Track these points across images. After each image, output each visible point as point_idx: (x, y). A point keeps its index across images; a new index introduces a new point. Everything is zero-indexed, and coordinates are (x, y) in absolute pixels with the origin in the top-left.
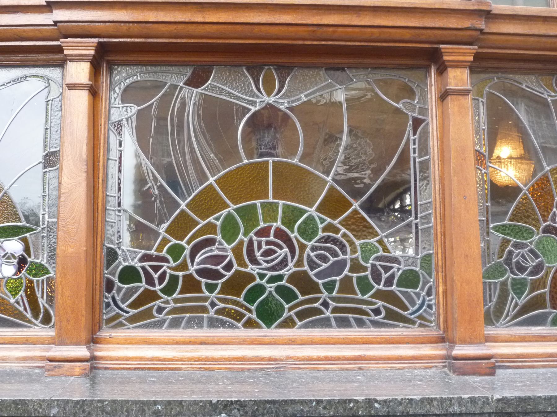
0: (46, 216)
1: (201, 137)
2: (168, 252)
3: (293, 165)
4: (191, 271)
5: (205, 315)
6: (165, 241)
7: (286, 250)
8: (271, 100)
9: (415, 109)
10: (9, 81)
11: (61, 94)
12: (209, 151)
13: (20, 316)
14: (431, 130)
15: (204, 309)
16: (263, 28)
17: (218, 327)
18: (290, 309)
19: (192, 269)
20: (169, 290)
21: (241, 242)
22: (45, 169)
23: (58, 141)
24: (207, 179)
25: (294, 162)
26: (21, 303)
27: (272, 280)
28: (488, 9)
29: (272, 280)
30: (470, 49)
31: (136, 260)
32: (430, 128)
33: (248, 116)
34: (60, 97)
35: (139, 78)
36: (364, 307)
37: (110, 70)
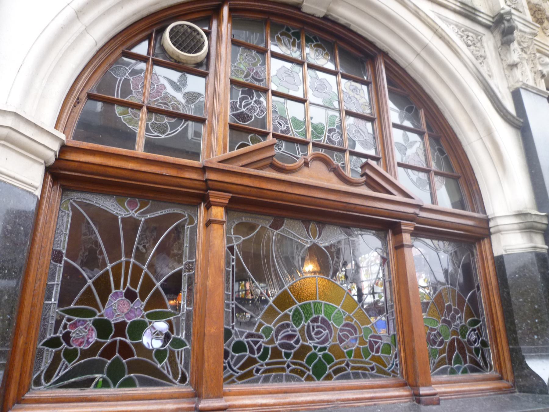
0: (185, 306)
2: (263, 331)
4: (276, 345)
5: (284, 373)
6: (261, 325)
7: (327, 331)
13: (164, 377)
15: (283, 370)
17: (290, 381)
18: (330, 368)
19: (277, 343)
20: (263, 358)
21: (303, 327)
26: (166, 368)
27: (321, 350)
29: (321, 350)
31: (243, 337)
36: (366, 366)
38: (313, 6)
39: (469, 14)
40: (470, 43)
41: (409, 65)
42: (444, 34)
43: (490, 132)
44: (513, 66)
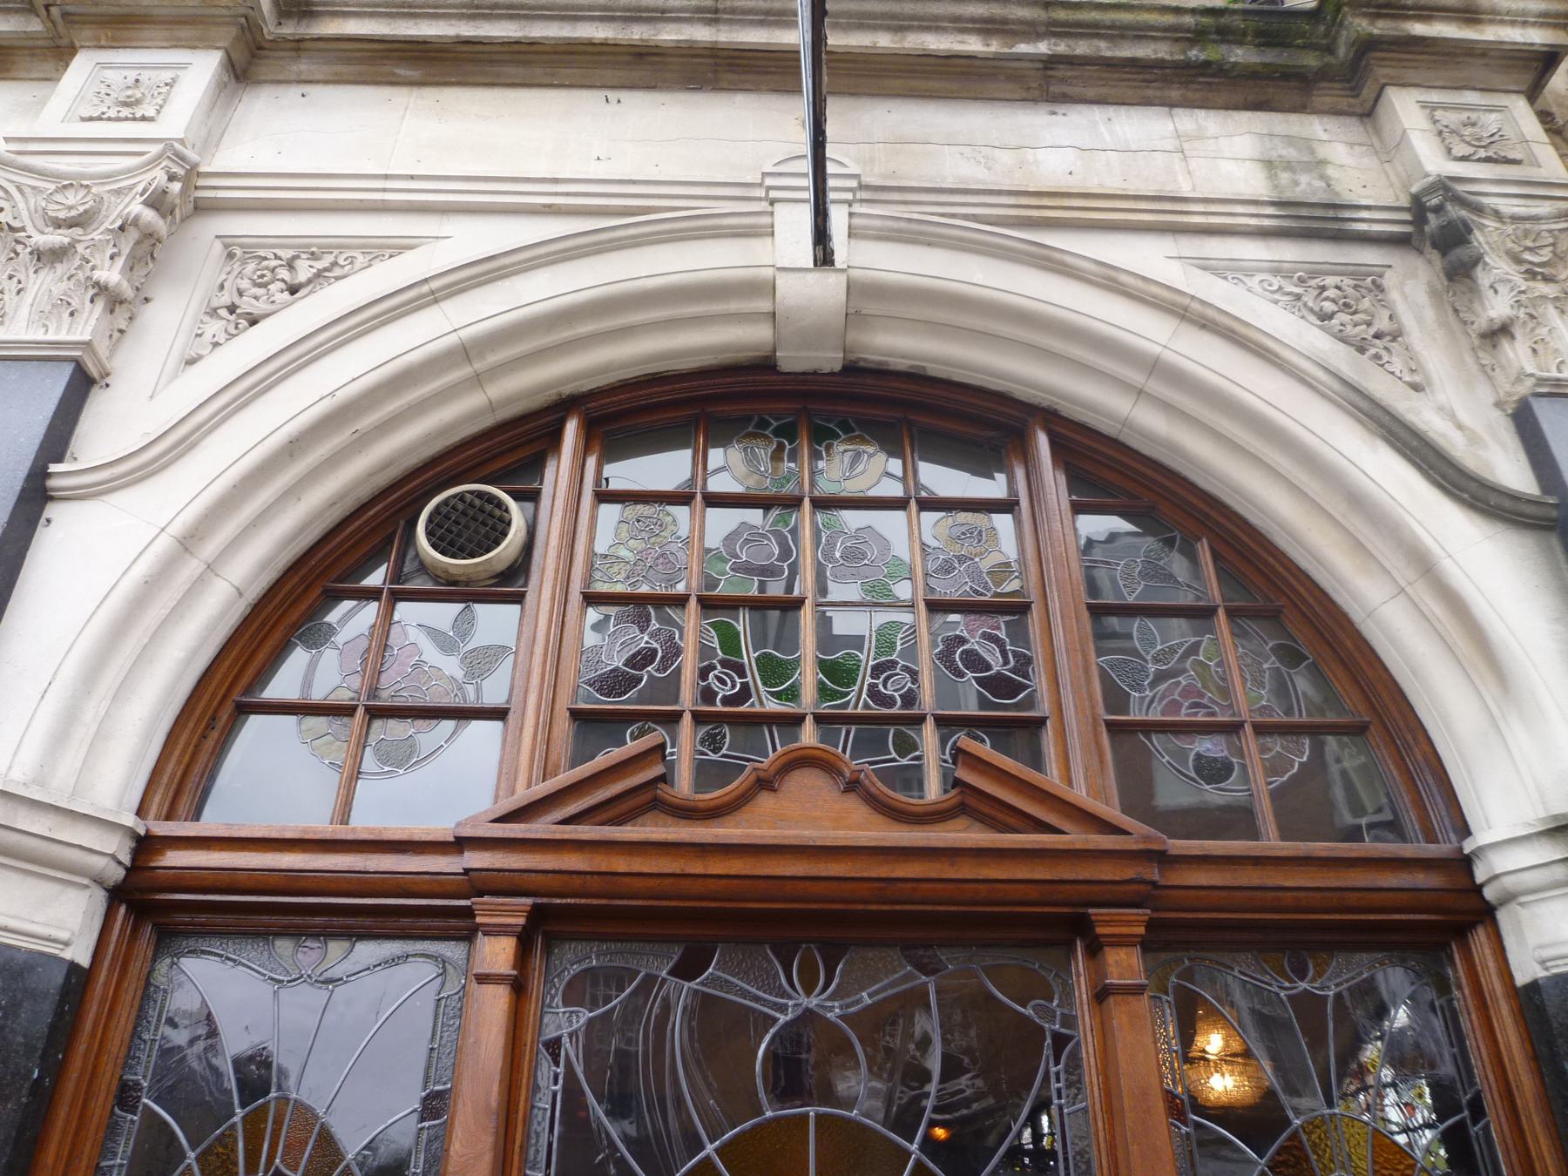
1: (693, 1066)
3: (849, 1121)
8: (813, 1002)
9: (1055, 1017)
10: (378, 962)
11: (464, 987)
12: (707, 1095)
14: (1084, 1056)
16: (801, 885)
22: (421, 1122)
23: (449, 1072)
24: (703, 1148)
25: (853, 1115)
28: (1163, 848)
30: (1138, 914)
32: (1084, 1052)
33: (772, 1031)
34: (461, 993)
35: (594, 963)
37: (548, 951)
38: (803, 354)
39: (1315, 225)
40: (1329, 307)
41: (1124, 425)
42: (1210, 313)
43: (1424, 566)
44: (1499, 333)
